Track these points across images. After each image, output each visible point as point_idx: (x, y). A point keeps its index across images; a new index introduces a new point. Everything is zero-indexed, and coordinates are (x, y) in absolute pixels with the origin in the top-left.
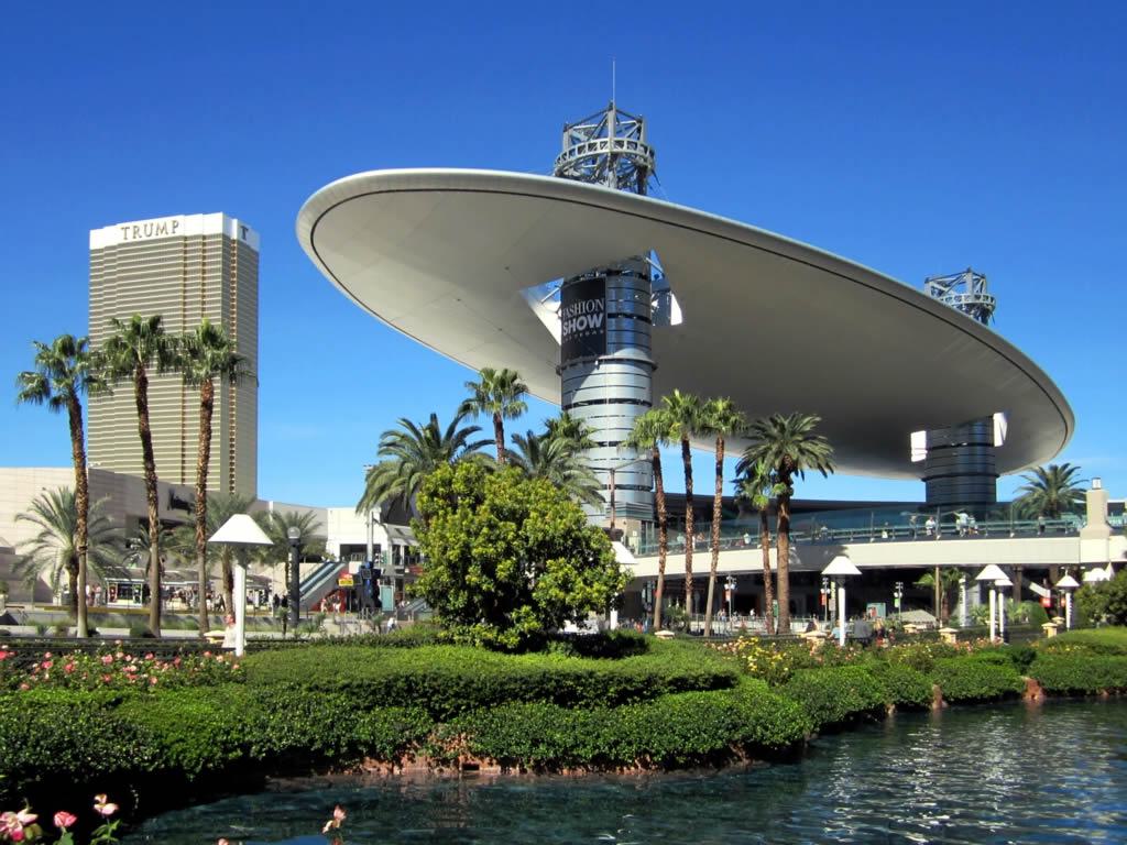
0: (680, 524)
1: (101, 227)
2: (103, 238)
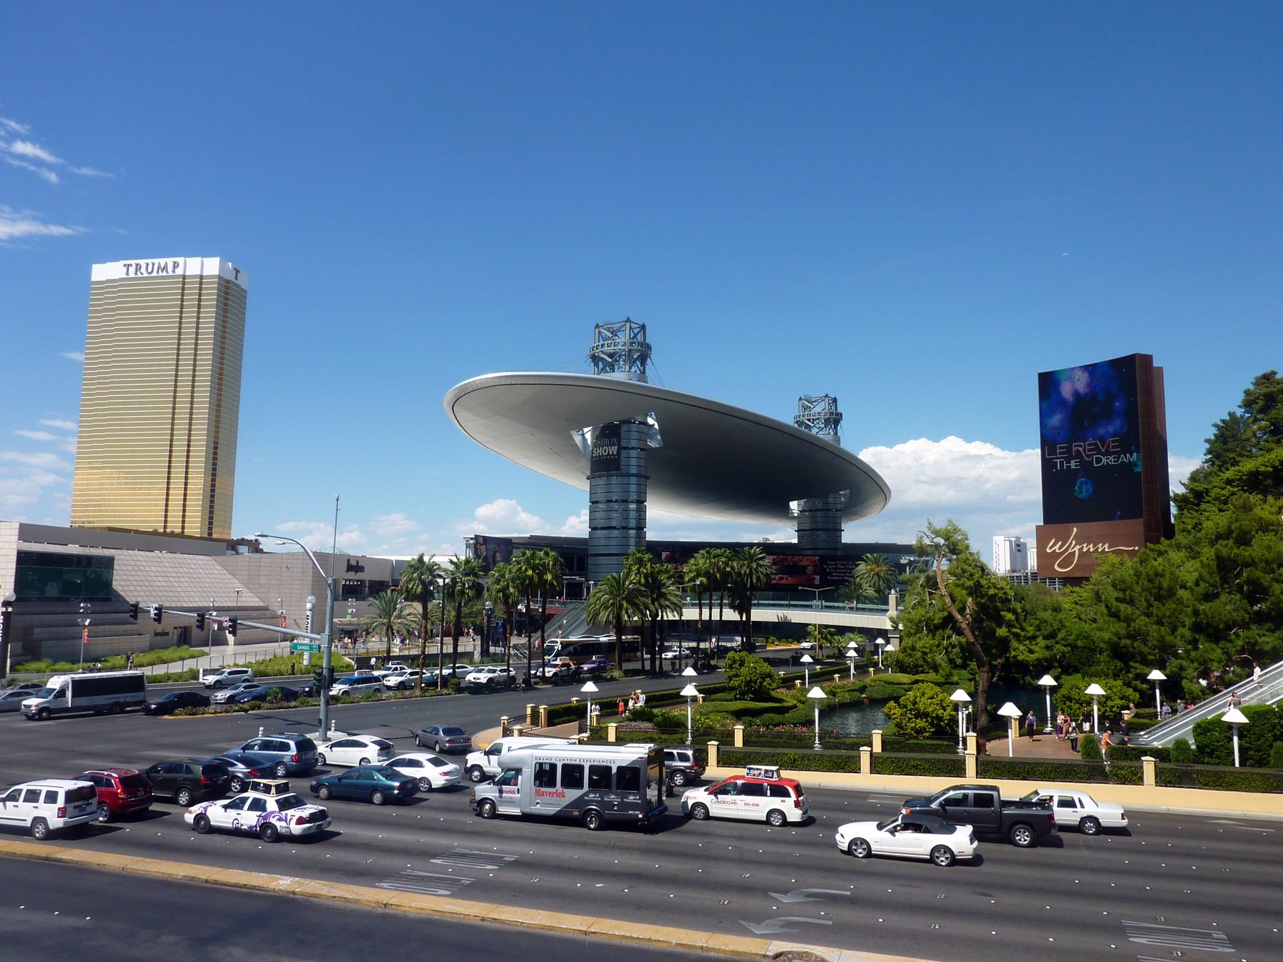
1: (103, 262)
2: (104, 272)
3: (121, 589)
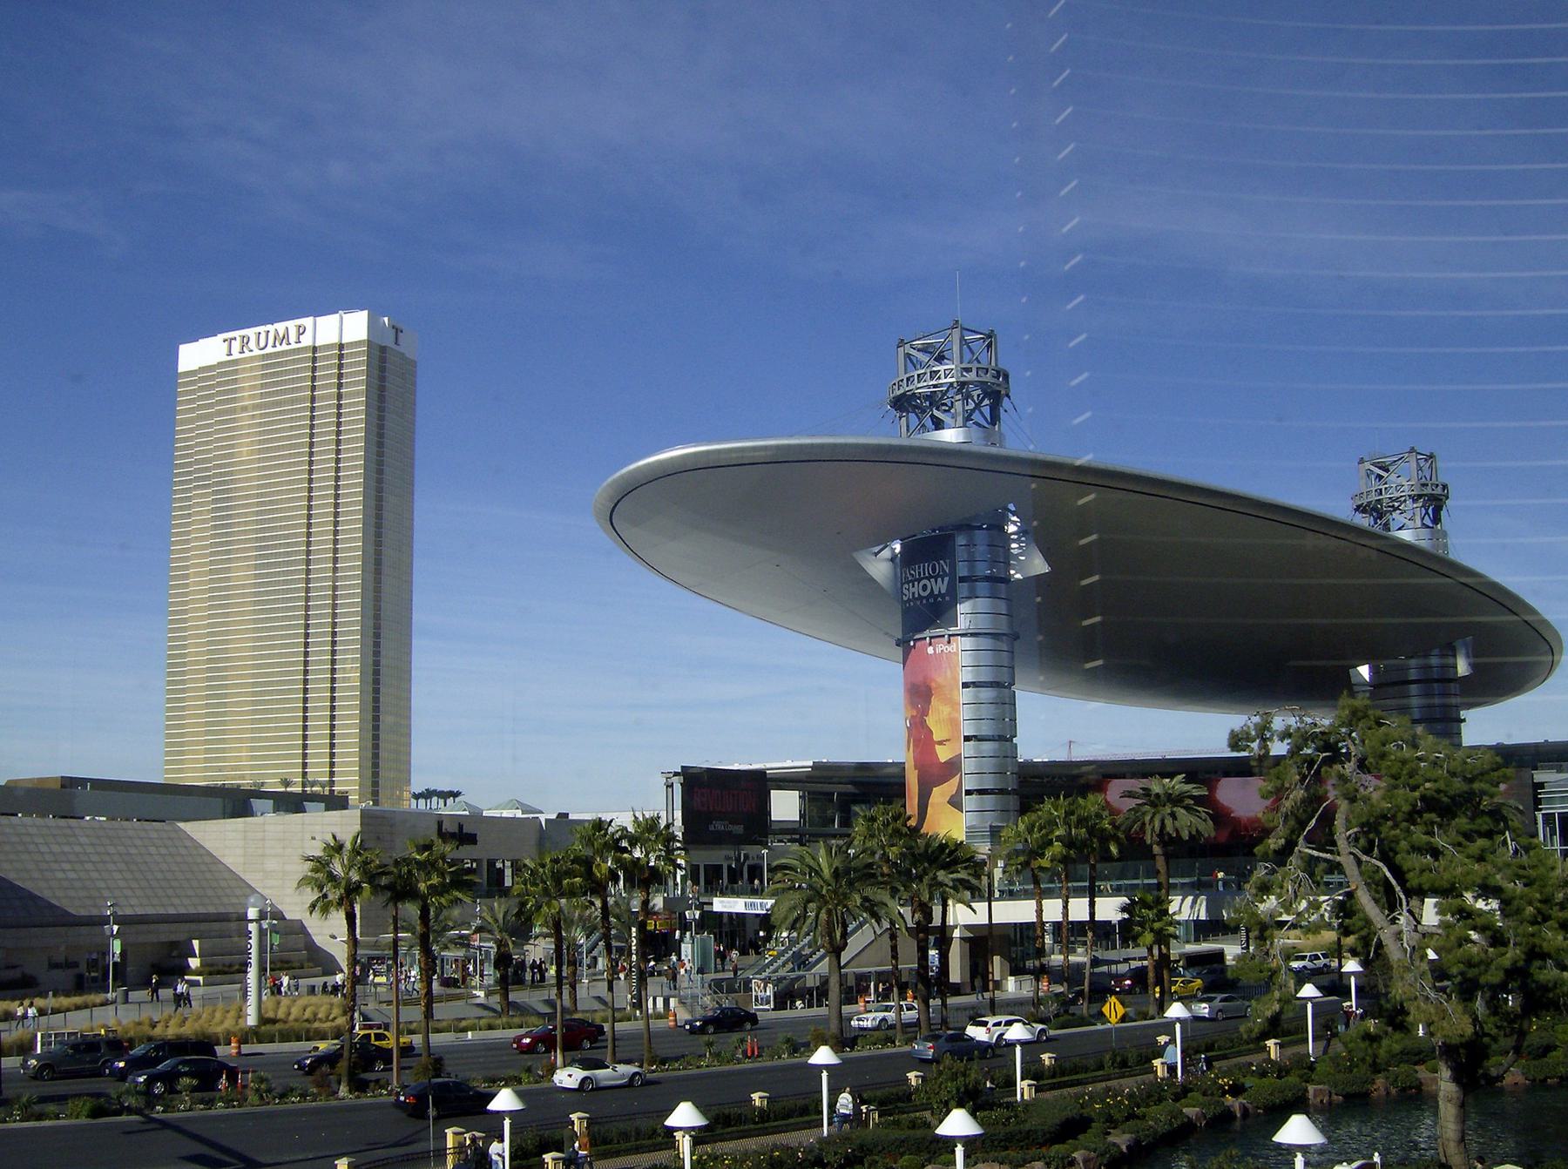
0: (892, 405)
2: (196, 355)
3: (120, 877)
